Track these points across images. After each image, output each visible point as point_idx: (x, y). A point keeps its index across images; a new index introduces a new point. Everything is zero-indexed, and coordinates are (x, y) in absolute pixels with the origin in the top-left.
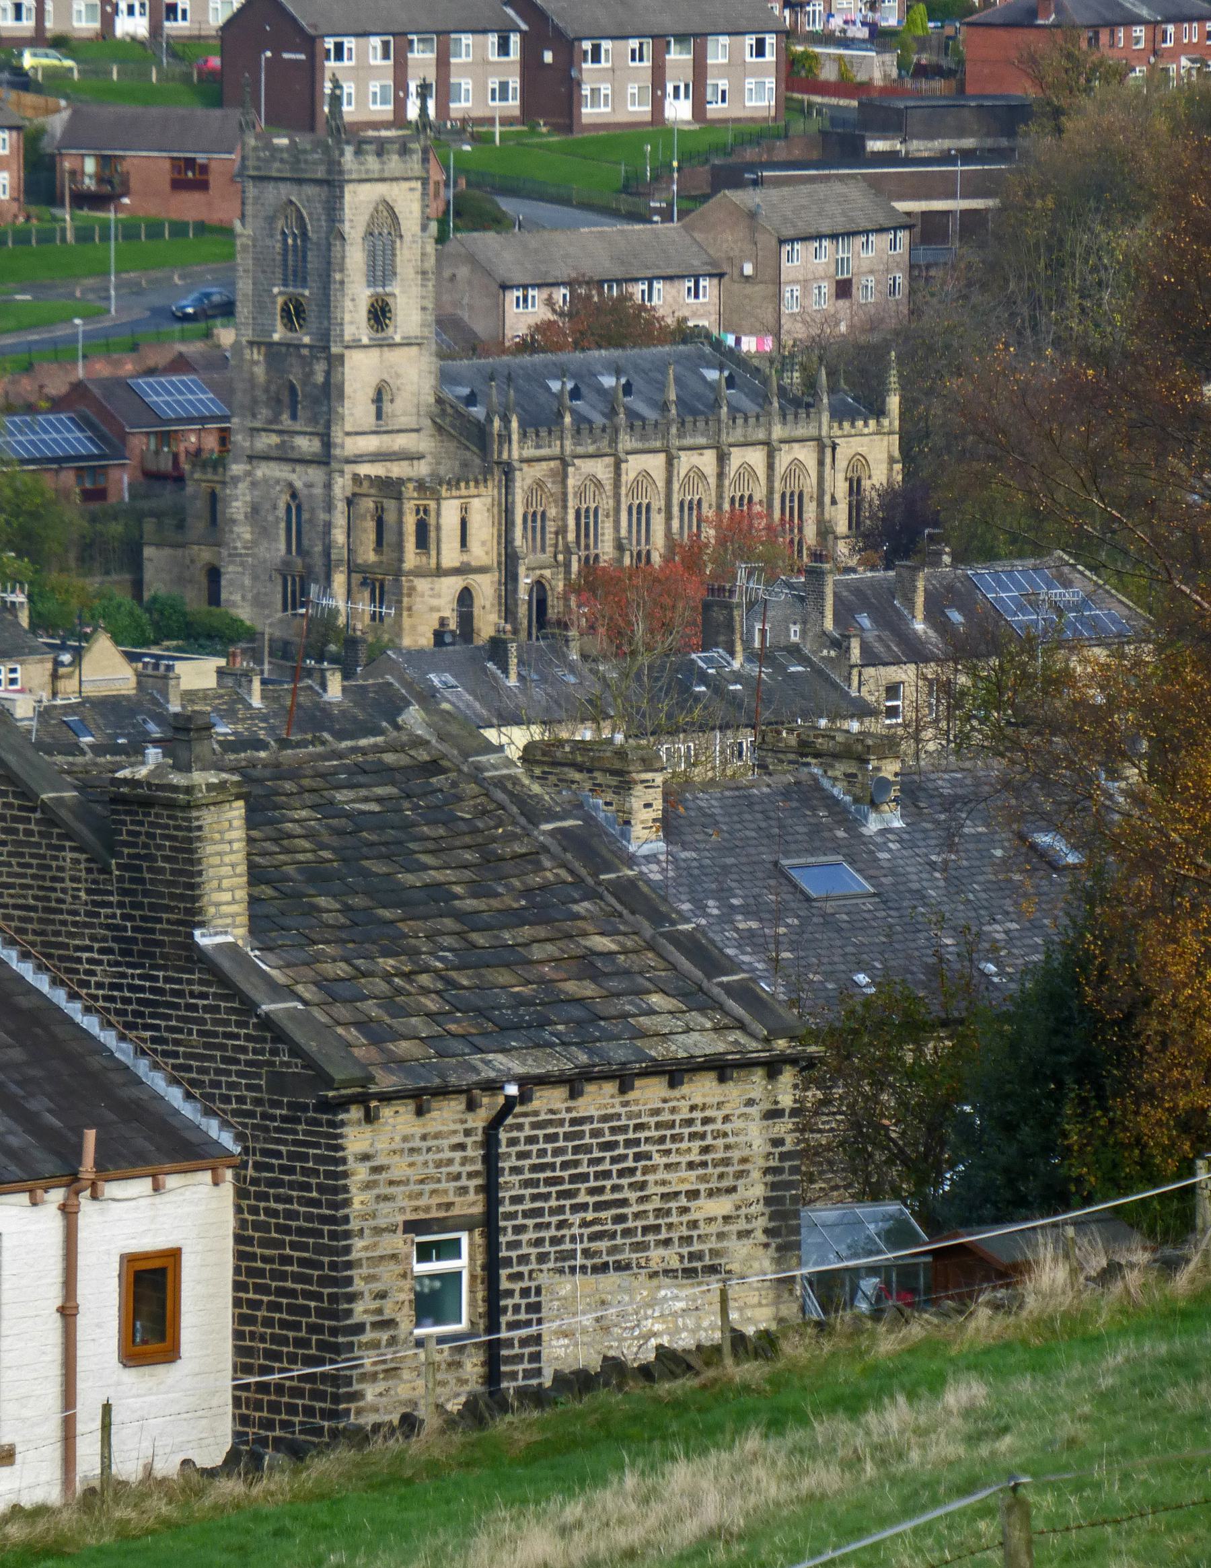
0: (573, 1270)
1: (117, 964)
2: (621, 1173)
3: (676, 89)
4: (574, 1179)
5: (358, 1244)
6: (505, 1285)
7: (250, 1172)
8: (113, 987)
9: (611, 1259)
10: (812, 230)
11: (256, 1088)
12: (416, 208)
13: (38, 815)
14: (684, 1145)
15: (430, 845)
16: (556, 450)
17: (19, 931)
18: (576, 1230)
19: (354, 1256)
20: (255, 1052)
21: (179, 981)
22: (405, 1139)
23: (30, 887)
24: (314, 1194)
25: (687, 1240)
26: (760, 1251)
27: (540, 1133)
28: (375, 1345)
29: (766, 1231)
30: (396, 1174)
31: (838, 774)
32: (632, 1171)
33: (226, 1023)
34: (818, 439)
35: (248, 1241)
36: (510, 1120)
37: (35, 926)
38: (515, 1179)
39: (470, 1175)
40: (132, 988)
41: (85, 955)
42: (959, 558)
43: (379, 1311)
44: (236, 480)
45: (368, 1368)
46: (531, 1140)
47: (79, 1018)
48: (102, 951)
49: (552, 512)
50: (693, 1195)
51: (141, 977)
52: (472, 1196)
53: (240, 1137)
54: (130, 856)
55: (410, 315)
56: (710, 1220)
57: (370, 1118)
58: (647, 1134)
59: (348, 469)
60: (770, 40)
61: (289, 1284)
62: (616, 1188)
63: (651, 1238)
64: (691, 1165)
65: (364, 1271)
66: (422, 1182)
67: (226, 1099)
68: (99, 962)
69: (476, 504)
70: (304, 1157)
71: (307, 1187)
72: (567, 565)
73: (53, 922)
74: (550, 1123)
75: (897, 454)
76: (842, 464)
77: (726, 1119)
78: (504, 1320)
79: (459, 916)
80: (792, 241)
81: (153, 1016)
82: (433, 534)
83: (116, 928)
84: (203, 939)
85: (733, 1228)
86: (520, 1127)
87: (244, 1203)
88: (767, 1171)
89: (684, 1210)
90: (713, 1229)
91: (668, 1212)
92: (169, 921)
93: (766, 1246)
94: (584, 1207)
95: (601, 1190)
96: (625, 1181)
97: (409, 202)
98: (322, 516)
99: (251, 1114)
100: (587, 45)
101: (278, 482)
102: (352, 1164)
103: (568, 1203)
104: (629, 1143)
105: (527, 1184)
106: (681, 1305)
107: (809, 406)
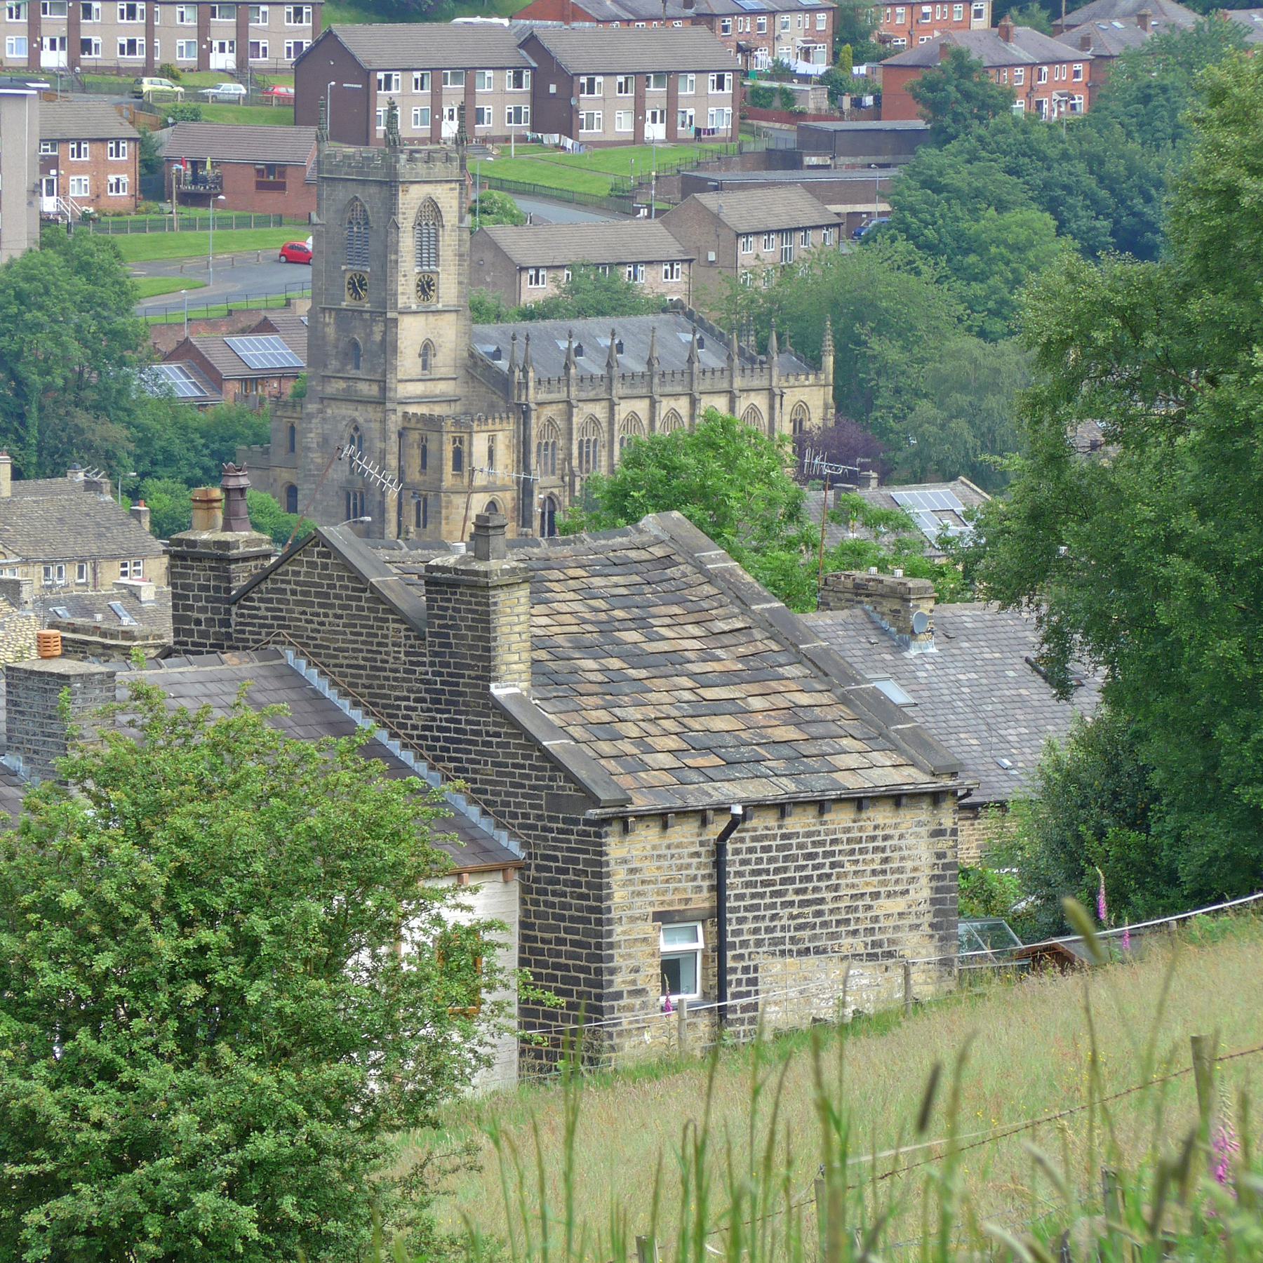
0: (783, 953)
1: (429, 710)
2: (820, 878)
3: (654, 114)
4: (784, 881)
5: (618, 929)
6: (730, 964)
7: (533, 873)
8: (425, 728)
9: (811, 945)
10: (761, 227)
11: (539, 807)
12: (455, 203)
13: (368, 594)
14: (869, 857)
15: (668, 621)
16: (563, 396)
17: (351, 685)
18: (785, 922)
19: (614, 939)
20: (537, 778)
21: (478, 723)
22: (654, 848)
23: (361, 651)
24: (584, 890)
25: (871, 931)
26: (927, 940)
27: (758, 845)
28: (630, 1008)
29: (931, 925)
30: (646, 875)
31: (886, 610)
32: (829, 876)
33: (514, 756)
34: (770, 390)
35: (530, 926)
36: (734, 835)
37: (364, 681)
38: (739, 880)
39: (704, 877)
40: (440, 729)
41: (404, 703)
42: (882, 482)
43: (634, 982)
44: (310, 416)
45: (625, 1026)
46: (751, 850)
47: (397, 752)
48: (417, 700)
49: (561, 443)
50: (876, 895)
51: (447, 720)
52: (705, 894)
53: (524, 845)
54: (440, 626)
55: (448, 288)
56: (888, 916)
57: (626, 830)
58: (840, 847)
59: (400, 409)
60: (728, 77)
61: (563, 961)
62: (815, 890)
63: (842, 929)
64: (874, 872)
65: (623, 951)
66: (667, 881)
67: (514, 816)
68: (414, 709)
69: (500, 436)
70: (575, 861)
71: (579, 885)
72: (572, 485)
73: (378, 678)
74: (766, 837)
75: (831, 401)
76: (788, 408)
77: (901, 837)
78: (729, 991)
79: (691, 675)
80: (747, 235)
81: (456, 751)
82: (466, 460)
83: (428, 682)
84: (497, 690)
85: (906, 922)
86: (742, 840)
87: (528, 897)
88: (933, 878)
89: (869, 908)
90: (890, 923)
91: (856, 909)
92: (470, 677)
93: (931, 937)
94: (791, 904)
95: (804, 891)
96: (823, 884)
97: (448, 199)
98: (379, 445)
99: (534, 827)
100: (584, 80)
101: (344, 418)
102: (613, 867)
103: (779, 900)
104: (827, 854)
105: (748, 885)
106: (865, 981)
107: (762, 363)
